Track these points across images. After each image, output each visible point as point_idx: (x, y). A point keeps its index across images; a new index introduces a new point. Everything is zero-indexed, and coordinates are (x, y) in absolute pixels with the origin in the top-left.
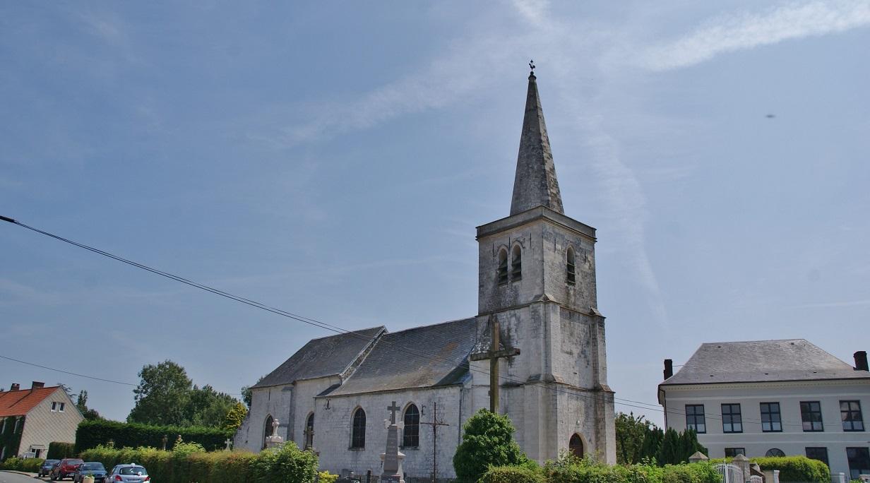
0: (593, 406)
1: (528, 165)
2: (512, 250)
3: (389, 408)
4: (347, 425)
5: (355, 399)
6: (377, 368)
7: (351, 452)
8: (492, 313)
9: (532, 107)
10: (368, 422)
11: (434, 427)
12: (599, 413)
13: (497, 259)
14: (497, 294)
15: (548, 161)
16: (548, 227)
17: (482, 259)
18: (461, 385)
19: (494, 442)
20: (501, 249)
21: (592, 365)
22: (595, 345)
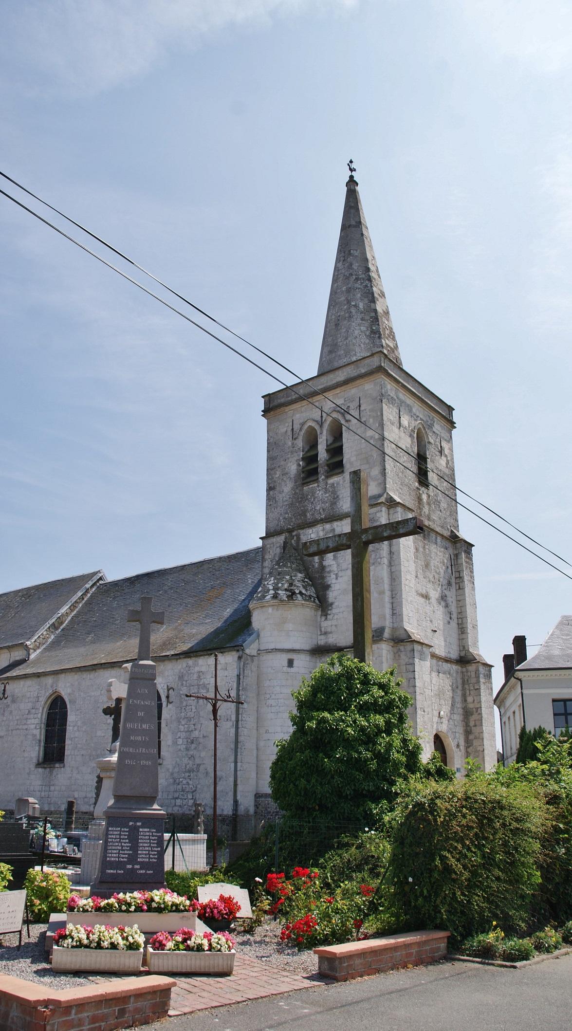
0: (460, 687)
1: (349, 302)
2: (326, 426)
3: (107, 711)
4: (35, 726)
5: (49, 680)
6: (89, 633)
7: (40, 770)
8: (290, 531)
9: (353, 223)
10: (71, 718)
11: (214, 706)
12: (470, 699)
13: (300, 443)
14: (299, 499)
15: (380, 299)
16: (389, 387)
17: (273, 446)
18: (238, 648)
19: (377, 726)
20: (306, 427)
21: (456, 620)
22: (460, 588)
